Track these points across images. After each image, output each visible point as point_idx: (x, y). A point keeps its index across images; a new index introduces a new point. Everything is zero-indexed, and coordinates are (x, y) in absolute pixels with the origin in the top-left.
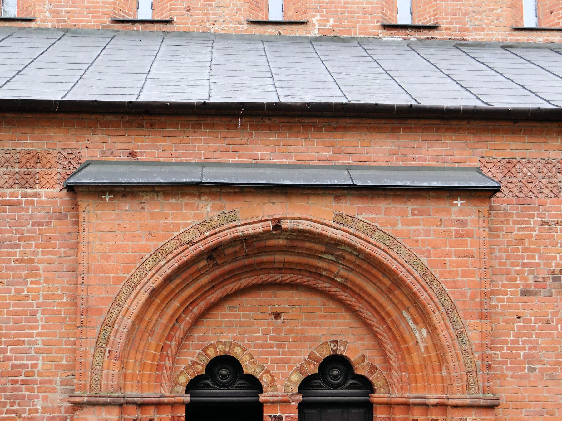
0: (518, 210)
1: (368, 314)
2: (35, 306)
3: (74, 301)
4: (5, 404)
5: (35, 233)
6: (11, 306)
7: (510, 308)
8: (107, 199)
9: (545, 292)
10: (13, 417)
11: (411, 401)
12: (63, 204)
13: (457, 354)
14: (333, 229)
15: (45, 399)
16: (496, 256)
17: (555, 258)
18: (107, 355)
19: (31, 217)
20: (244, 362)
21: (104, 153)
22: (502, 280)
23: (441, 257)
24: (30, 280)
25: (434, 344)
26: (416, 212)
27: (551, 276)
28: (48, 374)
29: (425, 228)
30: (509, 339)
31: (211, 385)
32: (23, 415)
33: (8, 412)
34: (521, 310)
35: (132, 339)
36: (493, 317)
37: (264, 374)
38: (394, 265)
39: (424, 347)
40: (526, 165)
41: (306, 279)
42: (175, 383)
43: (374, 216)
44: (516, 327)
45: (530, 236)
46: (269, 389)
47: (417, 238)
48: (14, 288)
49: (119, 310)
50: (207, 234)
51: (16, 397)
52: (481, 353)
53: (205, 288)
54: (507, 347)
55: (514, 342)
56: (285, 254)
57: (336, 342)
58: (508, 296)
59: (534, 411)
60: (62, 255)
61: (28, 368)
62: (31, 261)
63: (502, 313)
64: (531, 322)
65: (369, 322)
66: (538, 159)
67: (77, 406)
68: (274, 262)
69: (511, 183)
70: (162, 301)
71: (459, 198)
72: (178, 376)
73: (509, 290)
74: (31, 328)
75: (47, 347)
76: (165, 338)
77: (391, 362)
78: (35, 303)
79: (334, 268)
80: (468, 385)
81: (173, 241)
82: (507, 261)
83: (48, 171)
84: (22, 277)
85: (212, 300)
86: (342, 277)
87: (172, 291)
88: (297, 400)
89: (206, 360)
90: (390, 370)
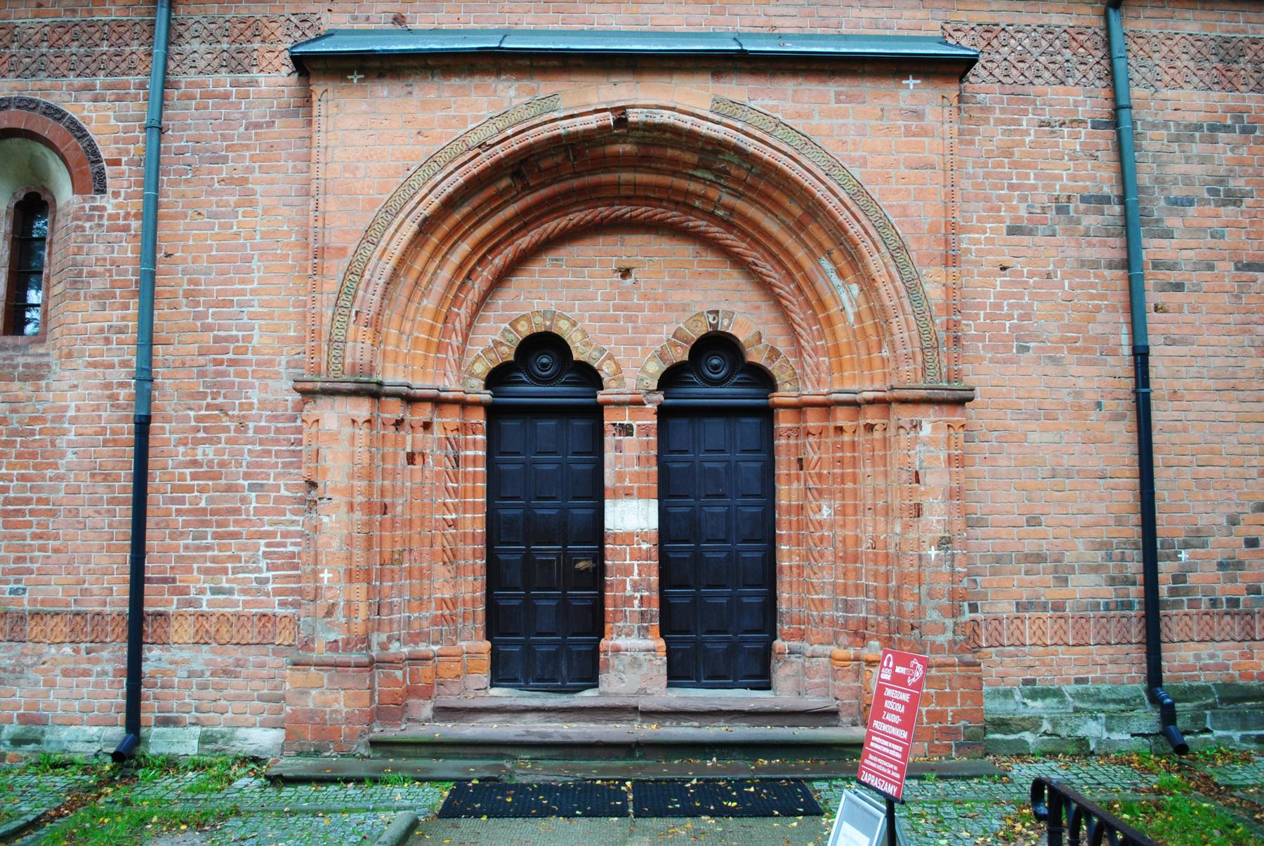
0: (1002, 102)
1: (767, 269)
4: (204, 396)
5: (250, 139)
8: (355, 81)
12: (291, 96)
13: (906, 320)
14: (710, 124)
15: (265, 388)
17: (1060, 178)
19: (245, 116)
20: (574, 343)
21: (355, 19)
23: (883, 167)
25: (870, 308)
26: (842, 97)
27: (1054, 205)
30: (988, 301)
31: (525, 379)
32: (230, 413)
33: (208, 407)
37: (604, 361)
38: (807, 181)
39: (855, 314)
41: (670, 214)
43: (775, 103)
44: (998, 283)
46: (613, 384)
47: (844, 138)
50: (510, 132)
51: (222, 385)
52: (945, 318)
53: (512, 225)
54: (986, 314)
56: (635, 171)
57: (717, 312)
59: (1025, 413)
61: (238, 341)
62: (245, 180)
63: (977, 261)
64: (1023, 276)
65: (768, 279)
66: (1033, 26)
68: (619, 185)
69: (992, 61)
73: (989, 226)
74: (243, 282)
75: (266, 310)
77: (802, 341)
79: (713, 193)
80: (924, 369)
81: (456, 142)
83: (272, 47)
84: (230, 206)
85: (523, 246)
86: (725, 207)
87: (458, 226)
90: (801, 354)
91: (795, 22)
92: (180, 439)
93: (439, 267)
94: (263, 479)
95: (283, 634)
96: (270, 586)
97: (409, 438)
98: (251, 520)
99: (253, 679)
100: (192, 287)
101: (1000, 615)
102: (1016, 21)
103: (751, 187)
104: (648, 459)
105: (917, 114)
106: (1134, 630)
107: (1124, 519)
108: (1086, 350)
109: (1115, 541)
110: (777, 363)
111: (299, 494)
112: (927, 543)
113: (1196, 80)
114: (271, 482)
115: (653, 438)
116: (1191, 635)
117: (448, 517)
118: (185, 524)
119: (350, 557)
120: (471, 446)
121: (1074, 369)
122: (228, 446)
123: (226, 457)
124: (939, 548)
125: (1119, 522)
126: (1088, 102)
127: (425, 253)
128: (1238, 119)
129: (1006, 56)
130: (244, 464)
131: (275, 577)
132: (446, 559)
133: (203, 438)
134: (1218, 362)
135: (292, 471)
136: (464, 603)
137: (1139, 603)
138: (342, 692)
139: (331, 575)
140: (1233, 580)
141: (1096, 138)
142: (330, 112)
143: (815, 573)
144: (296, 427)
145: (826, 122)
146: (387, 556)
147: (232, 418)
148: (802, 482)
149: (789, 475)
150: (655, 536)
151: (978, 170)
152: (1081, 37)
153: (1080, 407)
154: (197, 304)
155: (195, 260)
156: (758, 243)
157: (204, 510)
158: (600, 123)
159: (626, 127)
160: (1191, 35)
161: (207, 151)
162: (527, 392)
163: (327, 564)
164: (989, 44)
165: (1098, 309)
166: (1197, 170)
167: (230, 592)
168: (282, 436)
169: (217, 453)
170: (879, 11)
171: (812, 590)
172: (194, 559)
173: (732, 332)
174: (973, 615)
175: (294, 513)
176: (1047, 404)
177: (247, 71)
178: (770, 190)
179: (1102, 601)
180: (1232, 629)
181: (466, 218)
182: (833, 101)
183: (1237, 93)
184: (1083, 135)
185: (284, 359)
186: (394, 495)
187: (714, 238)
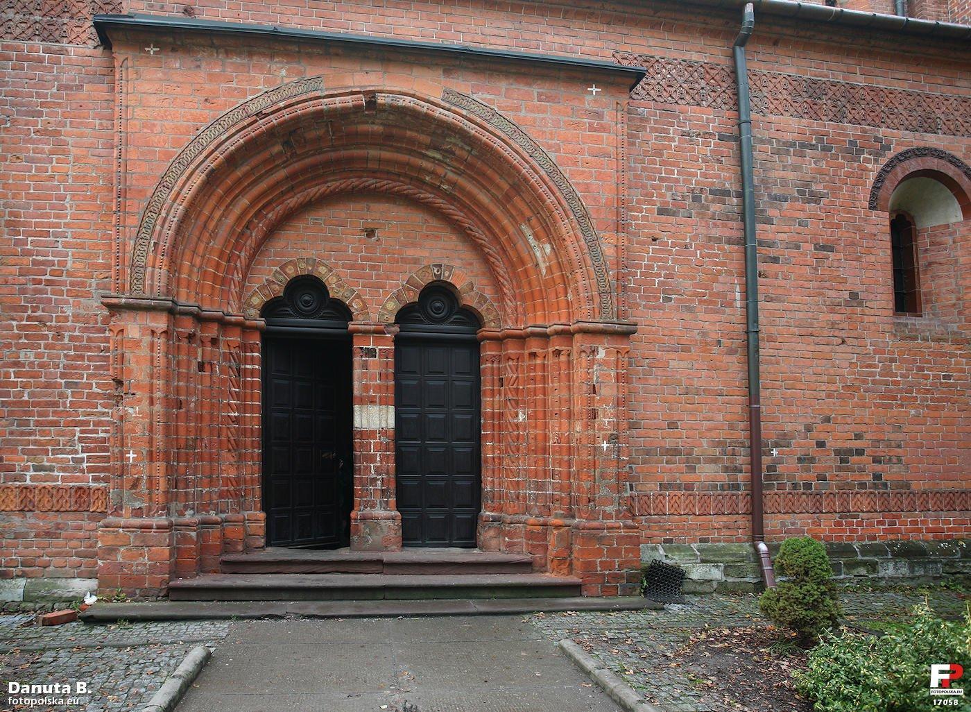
1: (480, 233)
4: (25, 309)
7: (646, 228)
8: (152, 53)
9: (684, 212)
19: (57, 79)
20: (330, 284)
32: (48, 324)
33: (29, 319)
34: (658, 231)
35: (187, 236)
37: (353, 299)
38: (516, 160)
40: (666, 65)
41: (405, 187)
43: (492, 97)
44: (651, 250)
46: (361, 317)
48: (35, 166)
49: (168, 192)
50: (282, 104)
51: (40, 301)
57: (440, 266)
58: (643, 214)
60: (97, 128)
61: (54, 265)
67: (114, 309)
73: (644, 207)
74: (57, 216)
77: (505, 289)
79: (440, 171)
81: (238, 110)
82: (642, 173)
83: (80, 23)
85: (291, 205)
86: (450, 182)
87: (239, 181)
91: (505, 41)
93: (223, 215)
95: (96, 504)
96: (85, 465)
97: (199, 351)
98: (67, 412)
100: (13, 219)
102: (667, 56)
103: (470, 166)
104: (387, 376)
105: (599, 115)
106: (741, 505)
107: (735, 425)
108: (711, 302)
109: (729, 440)
110: (485, 307)
112: (601, 438)
113: (792, 110)
116: (779, 508)
120: (249, 361)
121: (701, 316)
122: (46, 351)
123: (45, 359)
125: (732, 427)
127: (212, 202)
128: (820, 140)
134: (800, 315)
136: (245, 482)
138: (146, 549)
139: (135, 455)
140: (808, 470)
141: (722, 147)
142: (130, 78)
143: (513, 462)
145: (530, 115)
147: (50, 328)
148: (503, 396)
149: (493, 390)
150: (391, 432)
152: (712, 72)
153: (706, 344)
154: (18, 233)
156: (473, 212)
157: (27, 402)
159: (374, 109)
160: (789, 76)
165: (719, 273)
166: (790, 176)
167: (51, 469)
169: (38, 356)
170: (567, 38)
173: (451, 282)
176: (684, 340)
177: (57, 41)
178: (485, 168)
179: (719, 483)
180: (807, 504)
181: (247, 175)
182: (536, 100)
183: (820, 121)
186: (188, 394)
187: (440, 208)
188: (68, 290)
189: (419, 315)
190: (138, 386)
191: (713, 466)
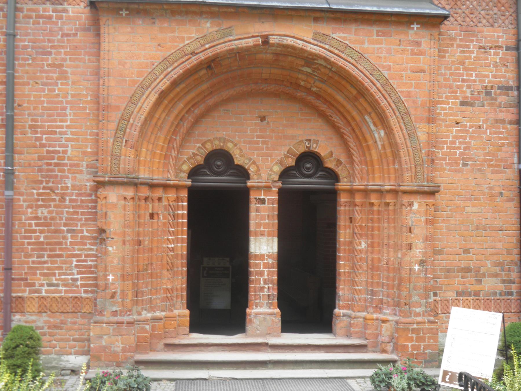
0: (461, 36)
2: (64, 103)
3: (97, 99)
4: (41, 182)
5: (64, 42)
6: (45, 103)
8: (124, 15)
10: (49, 193)
11: (370, 187)
13: (408, 150)
14: (312, 46)
15: (74, 179)
16: (442, 73)
17: (487, 76)
18: (124, 144)
19: (61, 29)
20: (235, 155)
22: (445, 93)
23: (399, 71)
24: (60, 81)
25: (392, 151)
26: (380, 33)
27: (484, 90)
28: (76, 159)
29: (387, 47)
30: (449, 140)
31: (208, 173)
33: (44, 188)
36: (438, 122)
37: (251, 165)
38: (361, 77)
39: (382, 145)
42: (179, 170)
43: (345, 35)
45: (470, 58)
47: (380, 55)
48: (48, 89)
51: (51, 177)
54: (447, 147)
55: (451, 142)
57: (310, 140)
58: (450, 106)
59: (465, 198)
61: (60, 153)
62: (61, 66)
67: (100, 185)
69: (456, 13)
70: (169, 102)
71: (415, 23)
72: (182, 165)
73: (451, 101)
74: (61, 121)
75: (75, 137)
76: (171, 133)
77: (354, 157)
78: (64, 101)
80: (416, 175)
84: (53, 79)
85: (210, 104)
87: (178, 93)
88: (278, 186)
89: (204, 152)
92: (29, 205)
94: (74, 227)
96: (79, 283)
97: (150, 206)
98: (68, 248)
99: (70, 330)
100: (34, 123)
101: (448, 298)
106: (513, 306)
108: (497, 166)
109: (506, 262)
111: (94, 235)
114: (79, 228)
115: (276, 206)
117: (170, 246)
118: (33, 250)
119: (123, 268)
120: (180, 208)
121: (489, 175)
122: (55, 209)
124: (419, 265)
125: (508, 252)
126: (505, 36)
129: (463, 10)
130: (64, 218)
131: (81, 278)
132: (169, 268)
133: (42, 205)
135: (90, 222)
136: (177, 290)
137: (516, 292)
138: (120, 337)
139: (113, 277)
141: (507, 56)
144: (92, 200)
146: (141, 268)
147: (57, 194)
148: (352, 229)
149: (345, 226)
151: (447, 71)
153: (492, 195)
154: (37, 132)
155: (35, 108)
156: (333, 105)
157: (42, 243)
158: (255, 43)
161: (40, 48)
162: (207, 179)
163: (111, 272)
164: (456, 4)
165: (503, 145)
167: (57, 285)
168: (84, 204)
169: (50, 212)
171: (355, 285)
172: (37, 268)
173: (318, 151)
174: (435, 298)
175: (91, 244)
177: (61, 4)
179: (498, 291)
184: (501, 54)
185: (84, 163)
188: (68, 170)
189: (295, 172)
190: (115, 233)
191: (494, 279)
